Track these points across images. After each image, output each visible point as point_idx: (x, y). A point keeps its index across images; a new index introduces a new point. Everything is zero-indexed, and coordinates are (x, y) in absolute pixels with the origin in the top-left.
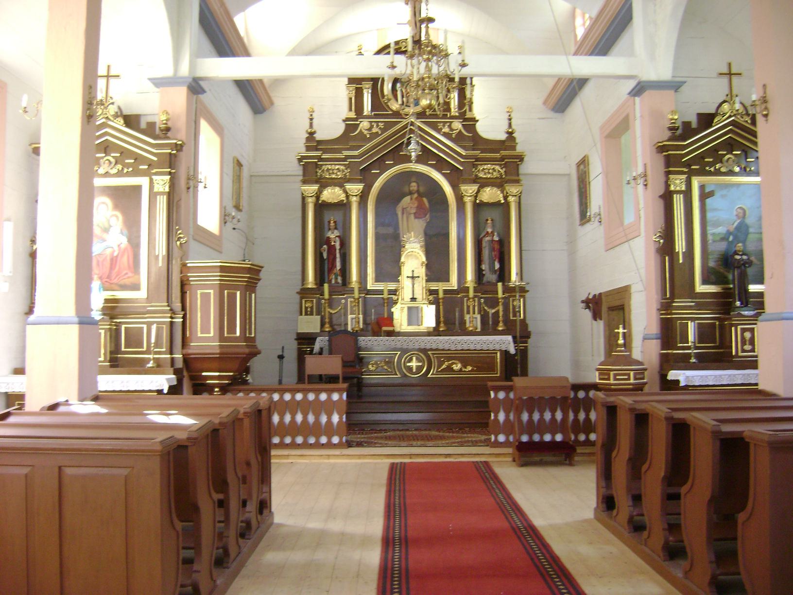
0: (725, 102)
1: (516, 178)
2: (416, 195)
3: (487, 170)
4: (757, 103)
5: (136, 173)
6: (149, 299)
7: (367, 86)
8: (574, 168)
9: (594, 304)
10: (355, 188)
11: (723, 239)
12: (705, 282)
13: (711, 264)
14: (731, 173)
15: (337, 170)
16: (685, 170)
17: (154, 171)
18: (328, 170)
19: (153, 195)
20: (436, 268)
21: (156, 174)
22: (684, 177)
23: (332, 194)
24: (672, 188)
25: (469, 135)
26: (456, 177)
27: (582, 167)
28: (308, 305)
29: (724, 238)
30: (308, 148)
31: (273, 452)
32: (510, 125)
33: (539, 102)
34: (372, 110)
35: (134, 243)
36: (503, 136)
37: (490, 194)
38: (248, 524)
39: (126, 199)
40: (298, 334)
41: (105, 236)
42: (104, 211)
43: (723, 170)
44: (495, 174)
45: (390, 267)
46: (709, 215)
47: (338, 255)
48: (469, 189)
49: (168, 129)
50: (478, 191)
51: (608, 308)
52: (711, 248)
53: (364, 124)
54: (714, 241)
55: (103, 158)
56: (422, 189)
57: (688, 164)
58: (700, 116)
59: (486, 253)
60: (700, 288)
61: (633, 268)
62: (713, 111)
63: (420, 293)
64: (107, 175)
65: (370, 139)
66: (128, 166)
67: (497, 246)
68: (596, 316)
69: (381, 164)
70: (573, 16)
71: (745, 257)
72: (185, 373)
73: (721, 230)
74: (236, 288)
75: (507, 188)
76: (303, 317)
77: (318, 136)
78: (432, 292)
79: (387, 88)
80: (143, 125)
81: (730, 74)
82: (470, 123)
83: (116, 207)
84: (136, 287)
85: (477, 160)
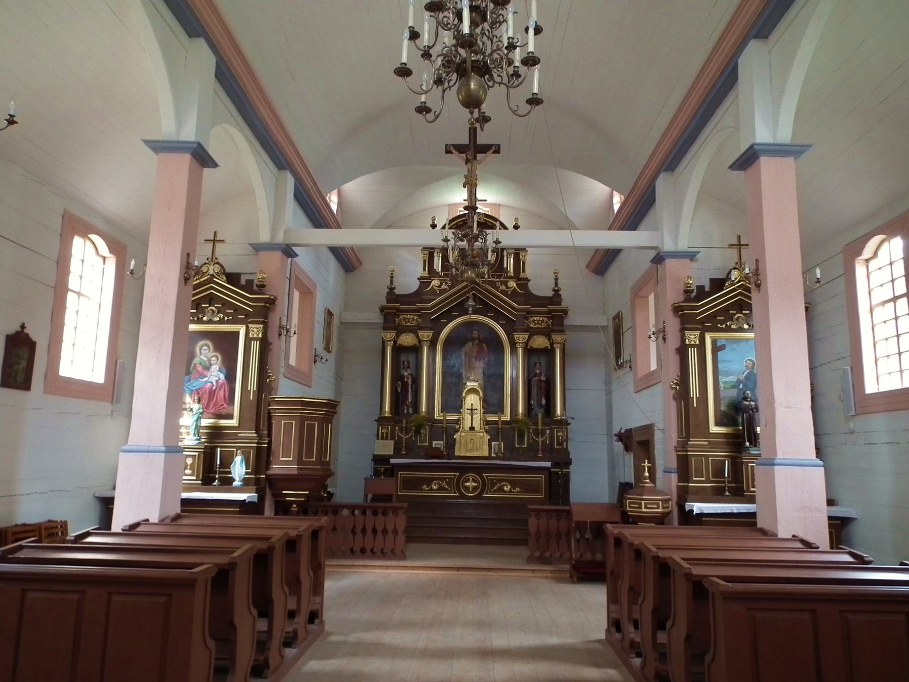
0: (735, 268)
1: (561, 328)
3: (536, 321)
4: (751, 275)
6: (240, 426)
8: (611, 321)
9: (626, 438)
10: (426, 335)
11: (733, 387)
12: (717, 424)
13: (723, 408)
15: (412, 319)
18: (404, 319)
19: (248, 340)
20: (492, 404)
21: (251, 323)
22: (698, 333)
23: (407, 339)
25: (524, 293)
30: (388, 301)
31: (326, 569)
32: (556, 284)
33: (583, 265)
35: (230, 377)
36: (550, 293)
37: (540, 342)
38: (295, 633)
39: (225, 344)
40: (374, 456)
41: (206, 372)
42: (205, 352)
43: (733, 327)
44: (544, 325)
45: (453, 402)
46: (720, 366)
48: (521, 337)
49: (263, 286)
50: (529, 339)
51: (638, 442)
52: (723, 394)
53: (435, 283)
56: (481, 337)
57: (702, 322)
59: (535, 390)
60: (714, 429)
61: (652, 409)
63: (477, 424)
64: (210, 322)
65: (440, 294)
66: (228, 315)
67: (543, 385)
68: (627, 448)
69: (449, 316)
70: (612, 196)
71: (752, 403)
72: (268, 491)
73: (732, 379)
74: (315, 419)
76: (380, 441)
77: (398, 291)
78: (488, 423)
80: (243, 282)
81: (740, 245)
82: (523, 283)
83: (217, 349)
84: (230, 417)
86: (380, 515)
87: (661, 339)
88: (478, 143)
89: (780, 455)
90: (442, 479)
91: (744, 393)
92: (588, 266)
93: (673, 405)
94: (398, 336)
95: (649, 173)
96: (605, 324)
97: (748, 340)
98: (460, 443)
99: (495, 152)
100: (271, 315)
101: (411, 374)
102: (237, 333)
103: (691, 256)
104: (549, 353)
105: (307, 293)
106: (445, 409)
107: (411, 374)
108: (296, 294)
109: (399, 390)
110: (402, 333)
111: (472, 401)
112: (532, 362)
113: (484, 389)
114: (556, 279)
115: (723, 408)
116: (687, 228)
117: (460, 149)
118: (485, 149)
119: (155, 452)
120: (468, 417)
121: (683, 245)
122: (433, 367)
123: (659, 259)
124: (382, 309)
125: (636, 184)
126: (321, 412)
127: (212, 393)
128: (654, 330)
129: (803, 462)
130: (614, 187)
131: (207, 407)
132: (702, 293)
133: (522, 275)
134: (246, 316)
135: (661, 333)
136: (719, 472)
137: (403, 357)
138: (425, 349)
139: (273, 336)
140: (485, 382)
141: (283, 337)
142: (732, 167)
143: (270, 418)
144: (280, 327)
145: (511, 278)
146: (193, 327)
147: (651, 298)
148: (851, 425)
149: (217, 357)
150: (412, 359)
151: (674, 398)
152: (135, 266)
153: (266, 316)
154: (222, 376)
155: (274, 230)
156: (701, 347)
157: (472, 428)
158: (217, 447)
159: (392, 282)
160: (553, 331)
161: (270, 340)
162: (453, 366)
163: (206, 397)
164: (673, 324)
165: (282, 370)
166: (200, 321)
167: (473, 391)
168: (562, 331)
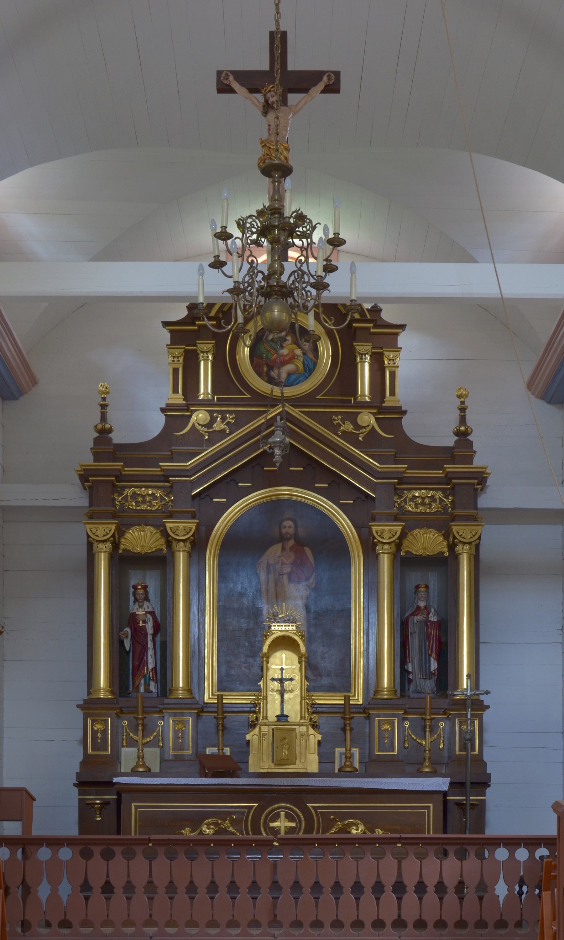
2: (291, 543)
7: (205, 348)
20: (325, 669)
23: (141, 539)
26: (362, 509)
28: (98, 727)
30: (97, 456)
32: (463, 420)
34: (214, 392)
36: (450, 441)
47: (150, 645)
48: (386, 531)
53: (200, 416)
56: (302, 532)
59: (414, 643)
63: (294, 706)
65: (211, 442)
67: (433, 632)
75: (455, 529)
77: (117, 438)
79: (424, 716)
85: (402, 481)
88: (290, 67)
90: (223, 815)
92: (530, 386)
94: (121, 532)
98: (260, 750)
101: (152, 613)
104: (445, 564)
106: (224, 684)
107: (152, 613)
110: (129, 526)
111: (283, 663)
112: (410, 586)
113: (309, 640)
114: (463, 410)
117: (252, 81)
118: (303, 82)
120: (274, 699)
122: (197, 625)
124: (85, 476)
133: (389, 401)
137: (135, 578)
140: (309, 625)
145: (364, 405)
150: (152, 582)
157: (282, 717)
160: (454, 518)
162: (241, 595)
168: (473, 518)
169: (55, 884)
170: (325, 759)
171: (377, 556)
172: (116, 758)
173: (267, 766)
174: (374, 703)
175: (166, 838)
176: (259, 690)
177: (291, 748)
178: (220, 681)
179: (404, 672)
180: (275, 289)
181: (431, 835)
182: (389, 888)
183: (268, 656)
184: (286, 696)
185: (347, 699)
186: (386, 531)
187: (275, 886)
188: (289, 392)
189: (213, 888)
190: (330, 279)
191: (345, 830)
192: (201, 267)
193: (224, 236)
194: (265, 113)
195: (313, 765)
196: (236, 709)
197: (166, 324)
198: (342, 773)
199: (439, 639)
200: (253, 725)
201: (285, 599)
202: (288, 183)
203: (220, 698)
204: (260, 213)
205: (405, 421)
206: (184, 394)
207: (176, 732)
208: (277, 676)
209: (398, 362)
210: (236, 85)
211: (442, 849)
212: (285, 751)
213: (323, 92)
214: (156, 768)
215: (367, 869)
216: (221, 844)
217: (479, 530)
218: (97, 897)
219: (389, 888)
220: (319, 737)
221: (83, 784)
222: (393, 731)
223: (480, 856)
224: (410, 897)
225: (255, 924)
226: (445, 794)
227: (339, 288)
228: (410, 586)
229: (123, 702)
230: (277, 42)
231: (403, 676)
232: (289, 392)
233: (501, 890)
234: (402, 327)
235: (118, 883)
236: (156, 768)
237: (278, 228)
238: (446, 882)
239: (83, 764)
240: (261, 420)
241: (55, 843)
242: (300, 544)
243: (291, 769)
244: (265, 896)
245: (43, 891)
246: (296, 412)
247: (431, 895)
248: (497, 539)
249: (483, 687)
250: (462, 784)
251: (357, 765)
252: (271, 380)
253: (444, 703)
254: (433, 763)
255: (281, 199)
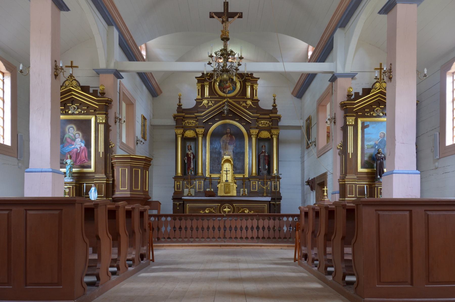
1: (277, 127)
2: (229, 135)
5: (88, 114)
6: (96, 172)
8: (305, 122)
10: (200, 131)
11: (372, 147)
12: (363, 167)
14: (378, 116)
16: (355, 115)
17: (97, 112)
19: (97, 124)
20: (238, 168)
21: (98, 114)
22: (354, 118)
23: (190, 134)
24: (348, 123)
26: (248, 126)
27: (308, 121)
29: (373, 147)
30: (178, 112)
32: (274, 103)
34: (209, 95)
35: (88, 145)
36: (271, 108)
37: (265, 134)
39: (84, 127)
41: (73, 142)
42: (72, 131)
43: (374, 115)
45: (216, 165)
46: (366, 136)
47: (192, 161)
48: (254, 132)
49: (104, 94)
51: (318, 184)
53: (205, 102)
54: (368, 148)
55: (71, 106)
56: (232, 132)
57: (357, 112)
58: (364, 90)
59: (262, 161)
62: (371, 87)
63: (230, 178)
64: (73, 114)
65: (208, 108)
66: (84, 110)
67: (267, 158)
68: (312, 189)
69: (213, 120)
71: (383, 155)
73: (372, 143)
74: (139, 168)
77: (184, 107)
78: (235, 179)
80: (91, 91)
82: (255, 102)
86: (178, 220)
87: (333, 123)
89: (396, 169)
90: (211, 207)
91: (378, 150)
92: (292, 93)
93: (338, 157)
94: (184, 132)
95: (330, 30)
96: (302, 125)
97: (382, 122)
98: (221, 189)
99: (239, 17)
100: (110, 111)
101: (192, 153)
102: (90, 121)
103: (352, 76)
104: (270, 140)
105: (131, 104)
106: (211, 172)
107: (192, 153)
108: (124, 105)
109: (186, 161)
110: (187, 130)
111: (227, 166)
112: (260, 146)
114: (274, 100)
115: (366, 159)
116: (352, 61)
117: (219, 15)
118: (233, 15)
119: (46, 172)
120: (224, 176)
121: (348, 70)
122: (204, 156)
123: (334, 78)
124: (175, 117)
125: (322, 38)
126: (142, 164)
127: (78, 154)
128: (329, 117)
129: (409, 172)
130: (310, 44)
131: (75, 162)
132: (357, 96)
133: (255, 98)
134: (95, 110)
135: (334, 120)
136: (362, 192)
137: (188, 144)
138: (200, 139)
139: (111, 122)
141: (118, 123)
142: (380, 12)
143: (113, 168)
144: (116, 118)
145: (248, 99)
146: (62, 117)
147: (328, 106)
148: (437, 164)
149: (79, 134)
150: (192, 144)
151: (339, 154)
152: (23, 68)
153: (107, 111)
154: (83, 145)
155: (108, 62)
156: (355, 126)
157: (227, 181)
158: (84, 183)
159: (180, 102)
160: (272, 128)
161: (110, 124)
162: (216, 148)
163: (74, 156)
164: (340, 114)
165: (118, 144)
166: (67, 114)
167: (227, 161)
168: (277, 128)
169: (166, 227)
170: (238, 192)
171: (252, 138)
172: (183, 192)
173: (223, 194)
174: (251, 177)
175: (196, 215)
176: (220, 173)
177: (229, 189)
178: (210, 171)
179: (259, 169)
180: (225, 70)
181: (266, 214)
182: (255, 228)
183: (223, 165)
184: (228, 175)
185: (244, 176)
186: (254, 132)
187: (225, 227)
188: (229, 95)
189: (208, 228)
190: (239, 68)
191: (243, 212)
192: (205, 64)
193: (211, 56)
194: (222, 23)
195: (235, 193)
196: (214, 179)
197: (196, 78)
198: (243, 196)
199: (268, 160)
200: (219, 183)
201: (227, 149)
202: (228, 42)
203: (210, 176)
204: (221, 50)
205: (259, 103)
206: (201, 95)
207: (199, 185)
208: (225, 170)
209: (257, 87)
210: (215, 16)
211: (269, 217)
212: (227, 190)
213: (238, 18)
214: (193, 195)
215: (249, 223)
216: (210, 216)
217: (279, 131)
218: (178, 231)
219: (255, 228)
220: (237, 186)
221: (174, 199)
222: (256, 185)
223: (280, 220)
224: (261, 230)
225: (219, 238)
226: (270, 202)
227: (242, 69)
228: (260, 146)
229: (185, 177)
230: (226, 5)
231: (259, 170)
232: (229, 95)
233: (285, 229)
234: (259, 78)
235: (183, 227)
236: (193, 195)
237: (225, 54)
238: (270, 227)
239: (174, 193)
240: (221, 103)
241: (166, 216)
242: (231, 135)
243: (229, 195)
244: (222, 230)
245: (163, 229)
246: (230, 101)
247: (266, 230)
248: (283, 134)
249: (280, 173)
250: (274, 199)
251: (246, 194)
252: (224, 92)
253: (269, 177)
254: (267, 193)
255: (226, 47)
